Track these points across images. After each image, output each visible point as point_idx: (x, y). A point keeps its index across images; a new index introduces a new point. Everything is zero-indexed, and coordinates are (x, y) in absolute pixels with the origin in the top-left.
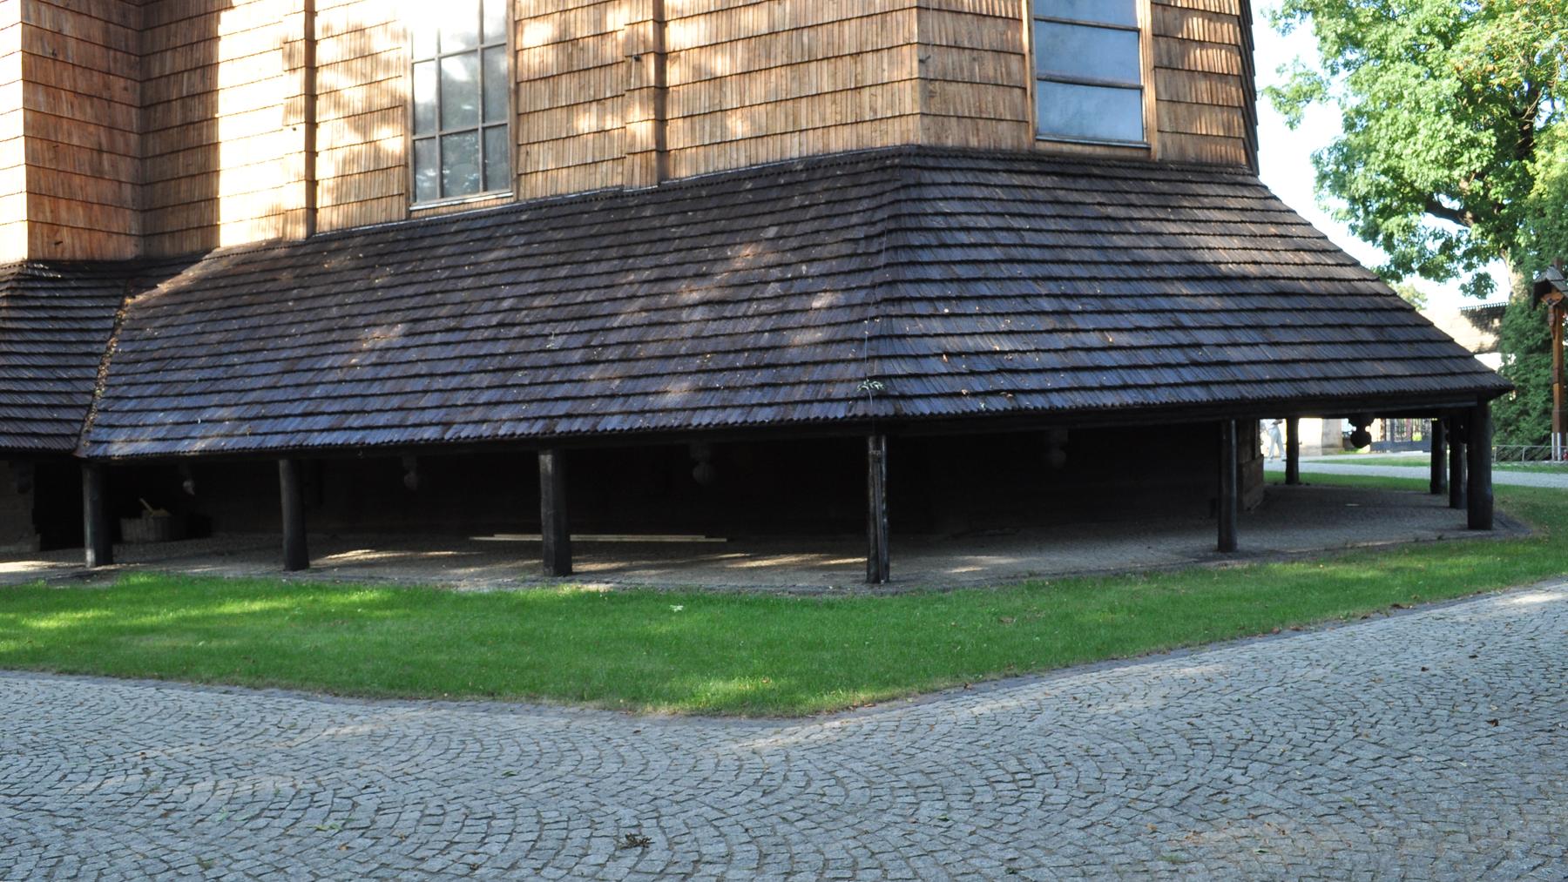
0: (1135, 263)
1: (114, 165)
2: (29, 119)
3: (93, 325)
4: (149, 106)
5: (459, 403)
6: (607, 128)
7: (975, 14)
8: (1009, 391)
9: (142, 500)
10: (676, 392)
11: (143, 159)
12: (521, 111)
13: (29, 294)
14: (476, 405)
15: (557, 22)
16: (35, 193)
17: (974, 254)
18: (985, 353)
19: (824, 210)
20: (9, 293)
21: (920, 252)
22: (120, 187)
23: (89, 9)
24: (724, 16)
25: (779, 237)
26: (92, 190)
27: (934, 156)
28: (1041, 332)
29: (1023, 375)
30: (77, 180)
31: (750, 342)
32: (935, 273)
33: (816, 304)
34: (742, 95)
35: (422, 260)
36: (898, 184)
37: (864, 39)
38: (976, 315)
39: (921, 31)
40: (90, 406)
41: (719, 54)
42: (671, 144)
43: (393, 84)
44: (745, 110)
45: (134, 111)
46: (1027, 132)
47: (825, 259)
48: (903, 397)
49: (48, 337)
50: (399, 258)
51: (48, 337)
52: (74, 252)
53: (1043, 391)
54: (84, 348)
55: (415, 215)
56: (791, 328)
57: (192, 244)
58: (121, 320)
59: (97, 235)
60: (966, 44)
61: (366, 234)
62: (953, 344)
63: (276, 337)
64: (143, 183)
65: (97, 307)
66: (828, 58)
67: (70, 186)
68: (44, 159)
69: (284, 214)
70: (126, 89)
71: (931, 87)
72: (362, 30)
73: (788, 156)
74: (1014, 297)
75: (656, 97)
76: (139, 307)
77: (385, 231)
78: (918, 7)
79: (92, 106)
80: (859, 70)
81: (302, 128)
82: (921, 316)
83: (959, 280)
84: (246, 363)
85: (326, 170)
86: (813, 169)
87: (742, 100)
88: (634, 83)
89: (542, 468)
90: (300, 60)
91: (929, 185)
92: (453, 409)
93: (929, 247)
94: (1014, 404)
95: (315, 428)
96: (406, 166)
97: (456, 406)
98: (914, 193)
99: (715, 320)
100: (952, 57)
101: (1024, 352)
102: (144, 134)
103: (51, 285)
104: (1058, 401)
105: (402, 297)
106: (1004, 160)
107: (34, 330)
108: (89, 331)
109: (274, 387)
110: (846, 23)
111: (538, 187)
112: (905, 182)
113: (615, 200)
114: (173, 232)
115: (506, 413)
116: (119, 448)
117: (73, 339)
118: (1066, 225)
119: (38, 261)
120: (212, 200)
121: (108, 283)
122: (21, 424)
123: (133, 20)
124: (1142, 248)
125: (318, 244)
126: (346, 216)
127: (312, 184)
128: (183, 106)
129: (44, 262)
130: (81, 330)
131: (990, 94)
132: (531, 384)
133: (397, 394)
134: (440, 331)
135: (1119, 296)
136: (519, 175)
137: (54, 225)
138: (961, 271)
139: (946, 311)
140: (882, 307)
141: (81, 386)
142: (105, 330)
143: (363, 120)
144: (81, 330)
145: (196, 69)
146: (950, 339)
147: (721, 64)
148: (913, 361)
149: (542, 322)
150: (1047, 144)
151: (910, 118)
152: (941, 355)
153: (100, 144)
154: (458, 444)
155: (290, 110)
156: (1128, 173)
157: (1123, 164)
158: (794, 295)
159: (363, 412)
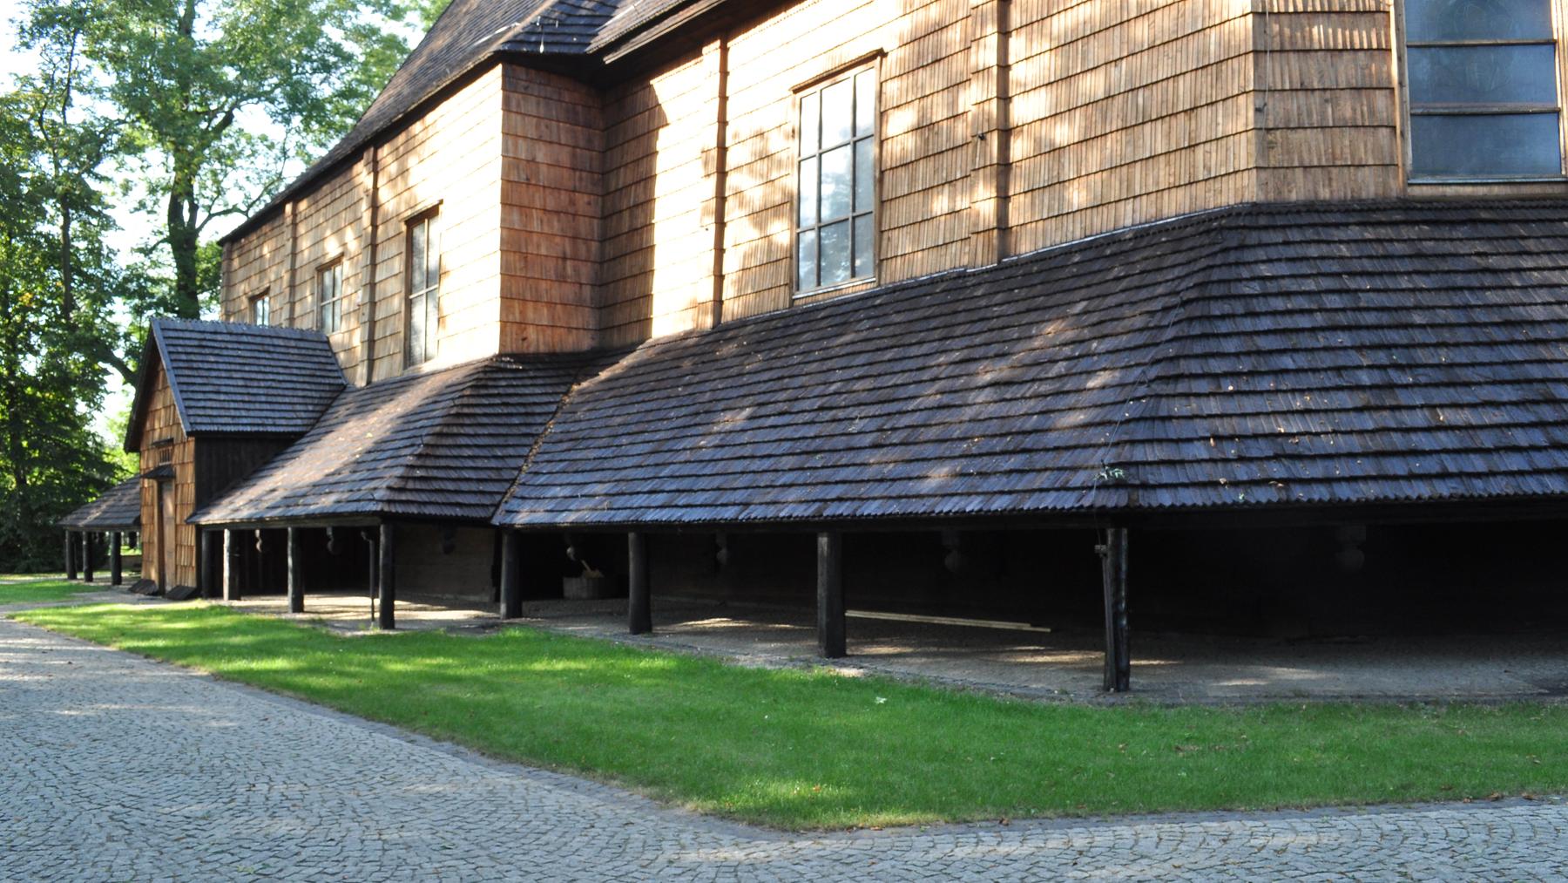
0: (1507, 323)
1: (576, 270)
3: (538, 410)
6: (957, 209)
7: (1328, 50)
8: (1279, 480)
10: (938, 476)
11: (601, 263)
12: (884, 198)
13: (490, 383)
15: (916, 109)
16: (506, 297)
17: (1287, 322)
18: (1265, 436)
19: (1136, 281)
21: (1219, 323)
24: (1064, 85)
25: (1085, 312)
26: (556, 292)
27: (1270, 214)
28: (1347, 410)
29: (1307, 462)
30: (544, 285)
31: (1018, 425)
32: (1230, 346)
33: (1091, 384)
34: (1079, 164)
35: (787, 346)
36: (1217, 248)
37: (1198, 92)
38: (1269, 392)
39: (1257, 78)
41: (1058, 125)
42: (1014, 219)
43: (783, 180)
44: (1083, 180)
45: (595, 221)
46: (1396, 177)
47: (1117, 335)
48: (1145, 486)
49: (496, 420)
50: (769, 345)
52: (538, 346)
53: (1328, 481)
55: (797, 303)
56: (1059, 410)
57: (632, 336)
60: (1316, 85)
61: (756, 323)
62: (1224, 427)
64: (600, 284)
65: (546, 394)
66: (1162, 118)
69: (697, 306)
70: (589, 203)
71: (1270, 137)
72: (762, 134)
73: (1121, 224)
74: (1325, 370)
75: (998, 174)
76: (581, 393)
77: (771, 319)
78: (1255, 52)
80: (1193, 126)
81: (713, 228)
82: (1198, 395)
83: (1259, 353)
85: (731, 265)
86: (1142, 236)
87: (1078, 170)
88: (979, 162)
89: (820, 550)
90: (713, 167)
91: (1254, 246)
93: (1232, 316)
94: (1283, 496)
96: (791, 257)
98: (1232, 257)
99: (995, 402)
100: (1295, 104)
101: (1317, 434)
102: (603, 240)
104: (1345, 492)
106: (1361, 211)
107: (485, 415)
108: (533, 414)
110: (1181, 78)
111: (897, 272)
112: (1226, 244)
113: (958, 281)
115: (793, 495)
116: (522, 518)
118: (1422, 282)
119: (506, 355)
120: (647, 297)
121: (561, 372)
122: (448, 495)
123: (597, 143)
124: (1524, 305)
125: (722, 331)
126: (745, 305)
127: (719, 278)
128: (631, 216)
130: (527, 414)
131: (1346, 139)
132: (823, 467)
135: (1473, 365)
136: (881, 261)
137: (522, 324)
138: (1264, 343)
139: (1231, 388)
140: (1154, 386)
141: (512, 463)
143: (761, 216)
144: (527, 414)
146: (1226, 420)
147: (1063, 133)
148: (1173, 446)
149: (854, 406)
150: (1425, 188)
151: (1246, 173)
152: (1208, 439)
153: (564, 253)
154: (751, 524)
155: (705, 212)
156: (1531, 215)
157: (1527, 204)
158: (1075, 374)
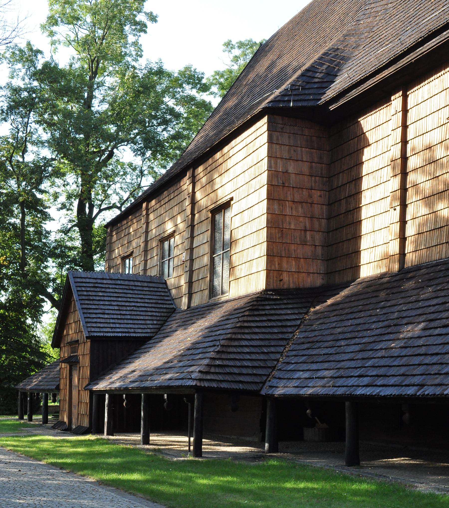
1: (312, 237)
2: (269, 218)
3: (289, 324)
4: (332, 204)
5: (432, 373)
9: (316, 418)
11: (328, 232)
14: (441, 374)
20: (250, 308)
22: (315, 248)
23: (302, 158)
26: (301, 251)
30: (293, 247)
40: (274, 367)
51: (264, 330)
54: (280, 336)
58: (305, 320)
59: (302, 275)
61: (427, 267)
63: (365, 330)
64: (327, 245)
67: (288, 250)
68: (276, 238)
70: (320, 196)
76: (316, 313)
77: (437, 265)
79: (302, 207)
84: (346, 345)
85: (411, 230)
90: (398, 171)
92: (429, 376)
95: (361, 384)
97: (431, 374)
103: (273, 303)
105: (430, 306)
107: (257, 327)
108: (286, 326)
109: (353, 360)
114: (340, 271)
116: (279, 392)
117: (276, 331)
119: (270, 290)
122: (235, 376)
126: (421, 257)
127: (403, 239)
129: (273, 290)
133: (405, 366)
134: (440, 327)
141: (273, 356)
142: (295, 326)
144: (282, 326)
145: (352, 181)
153: (305, 227)
154: (425, 398)
155: (393, 199)
159: (385, 376)
